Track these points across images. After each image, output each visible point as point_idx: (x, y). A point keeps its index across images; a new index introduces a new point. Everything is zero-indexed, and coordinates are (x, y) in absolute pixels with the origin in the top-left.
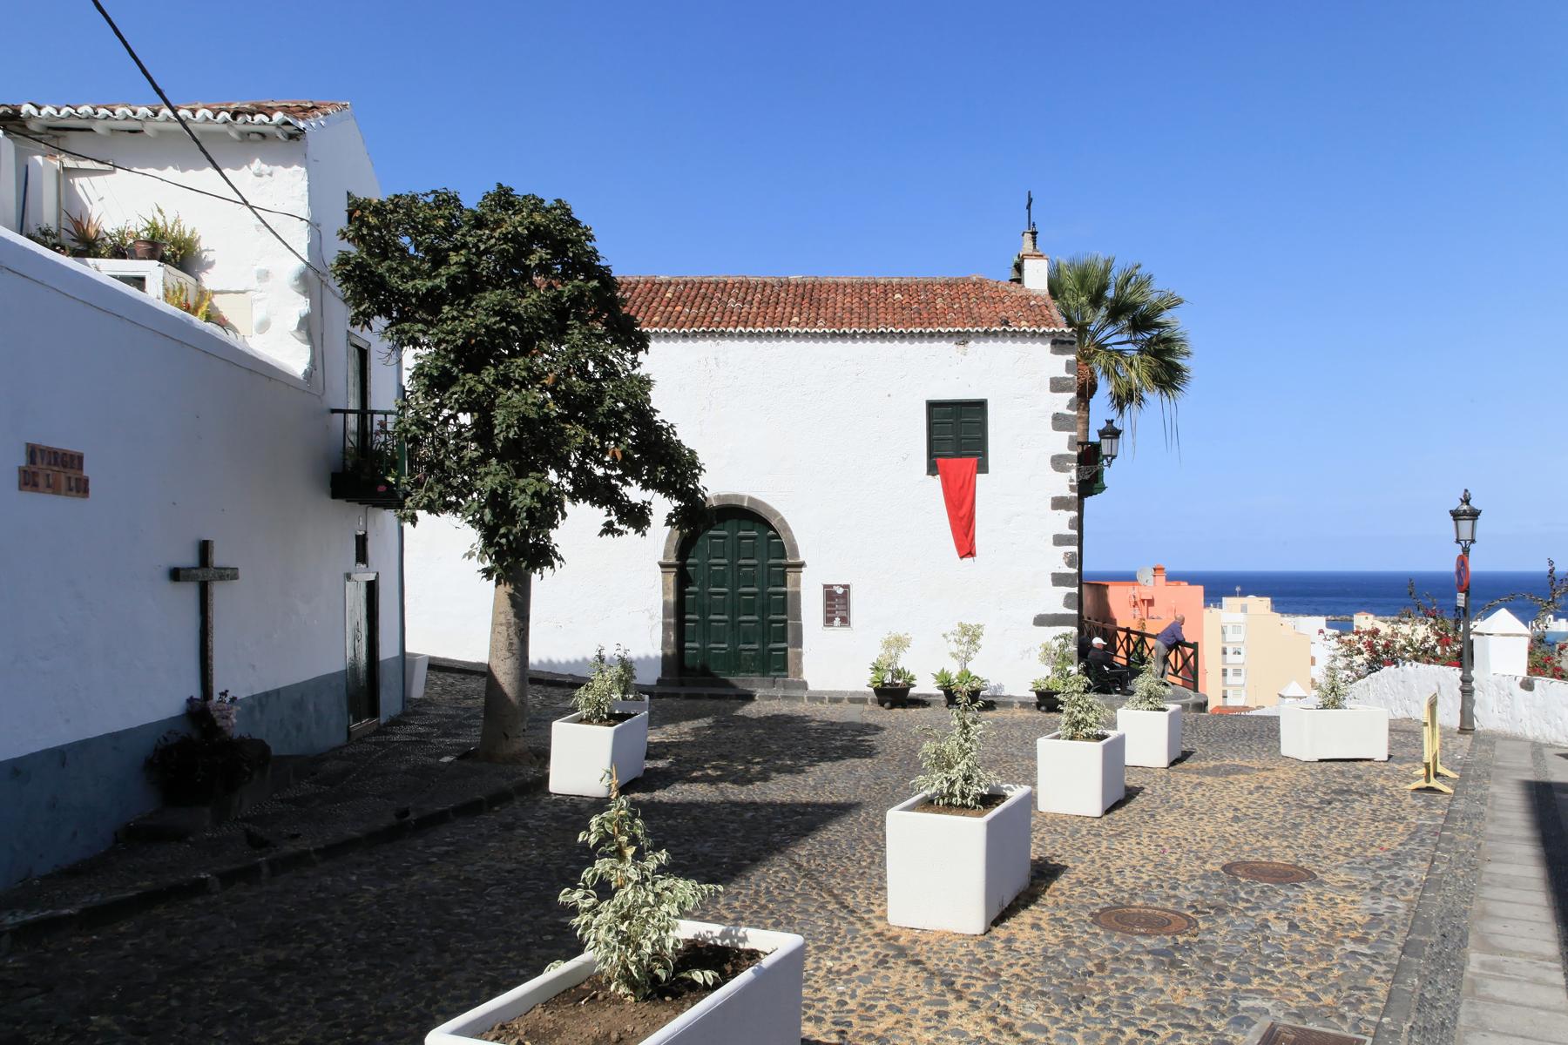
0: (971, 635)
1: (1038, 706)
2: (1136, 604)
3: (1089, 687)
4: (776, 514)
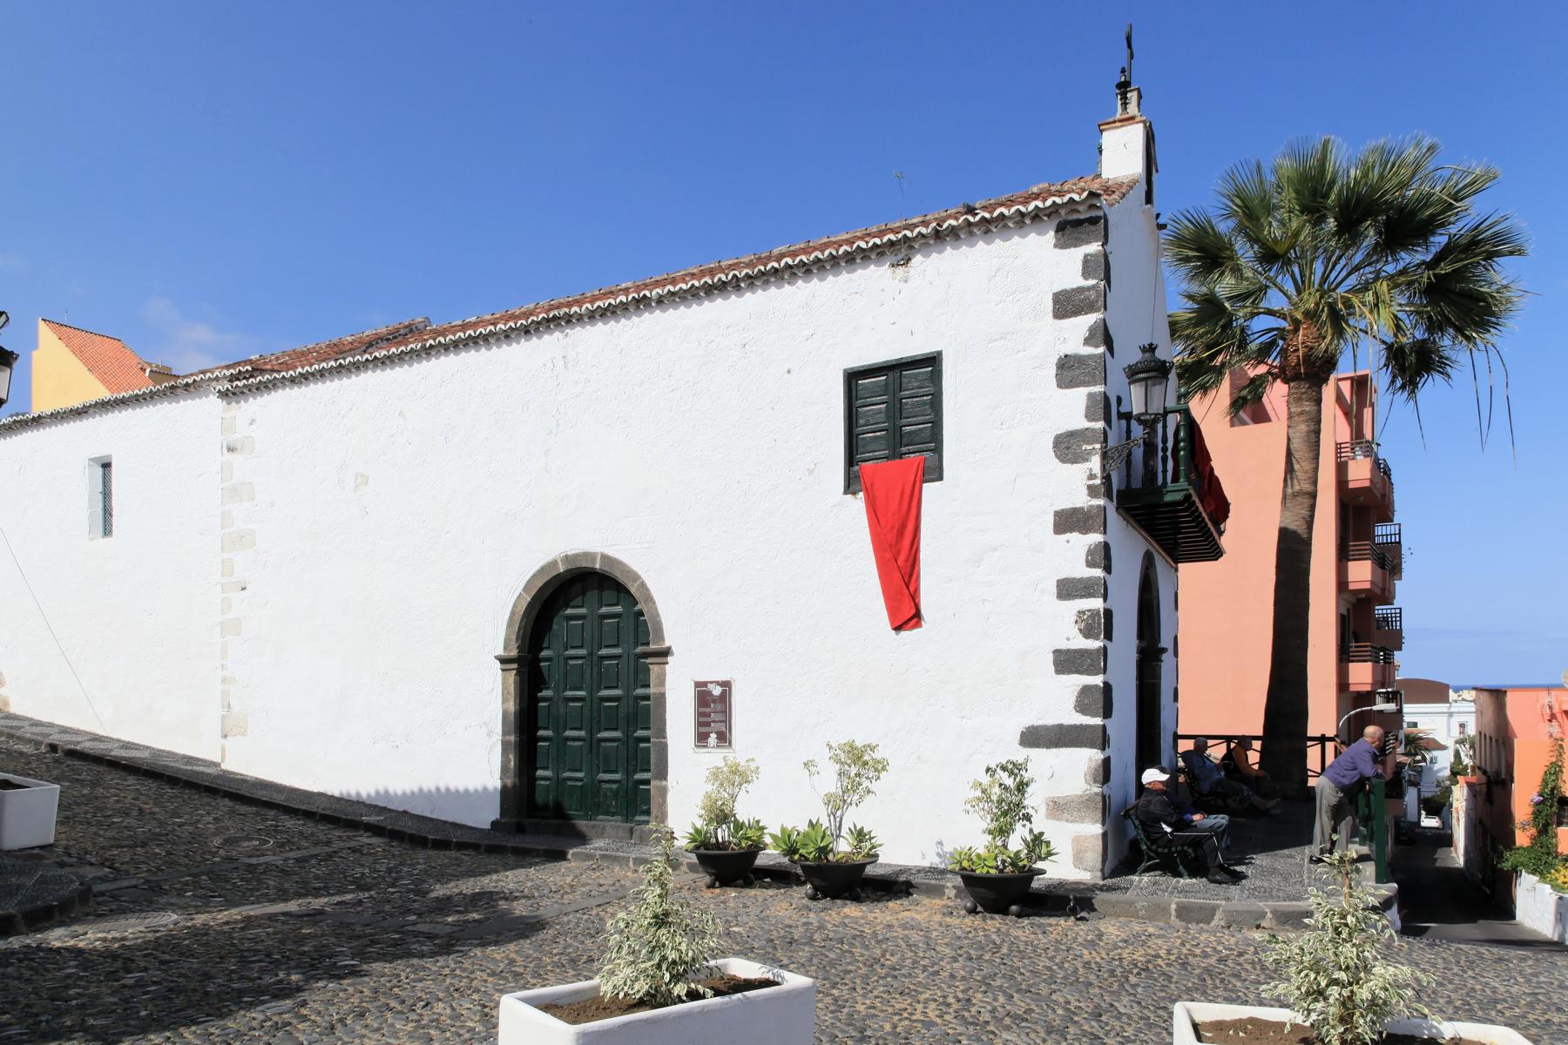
0: (859, 764)
2: (1553, 717)
4: (636, 577)
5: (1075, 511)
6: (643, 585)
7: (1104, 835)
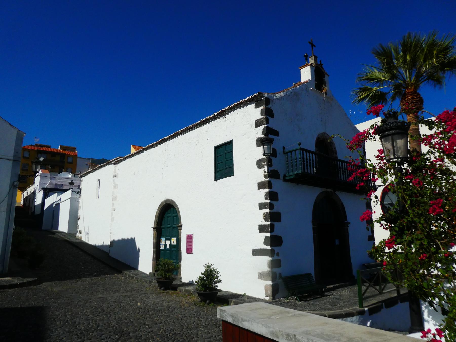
5: (262, 182)
7: (20, 207)
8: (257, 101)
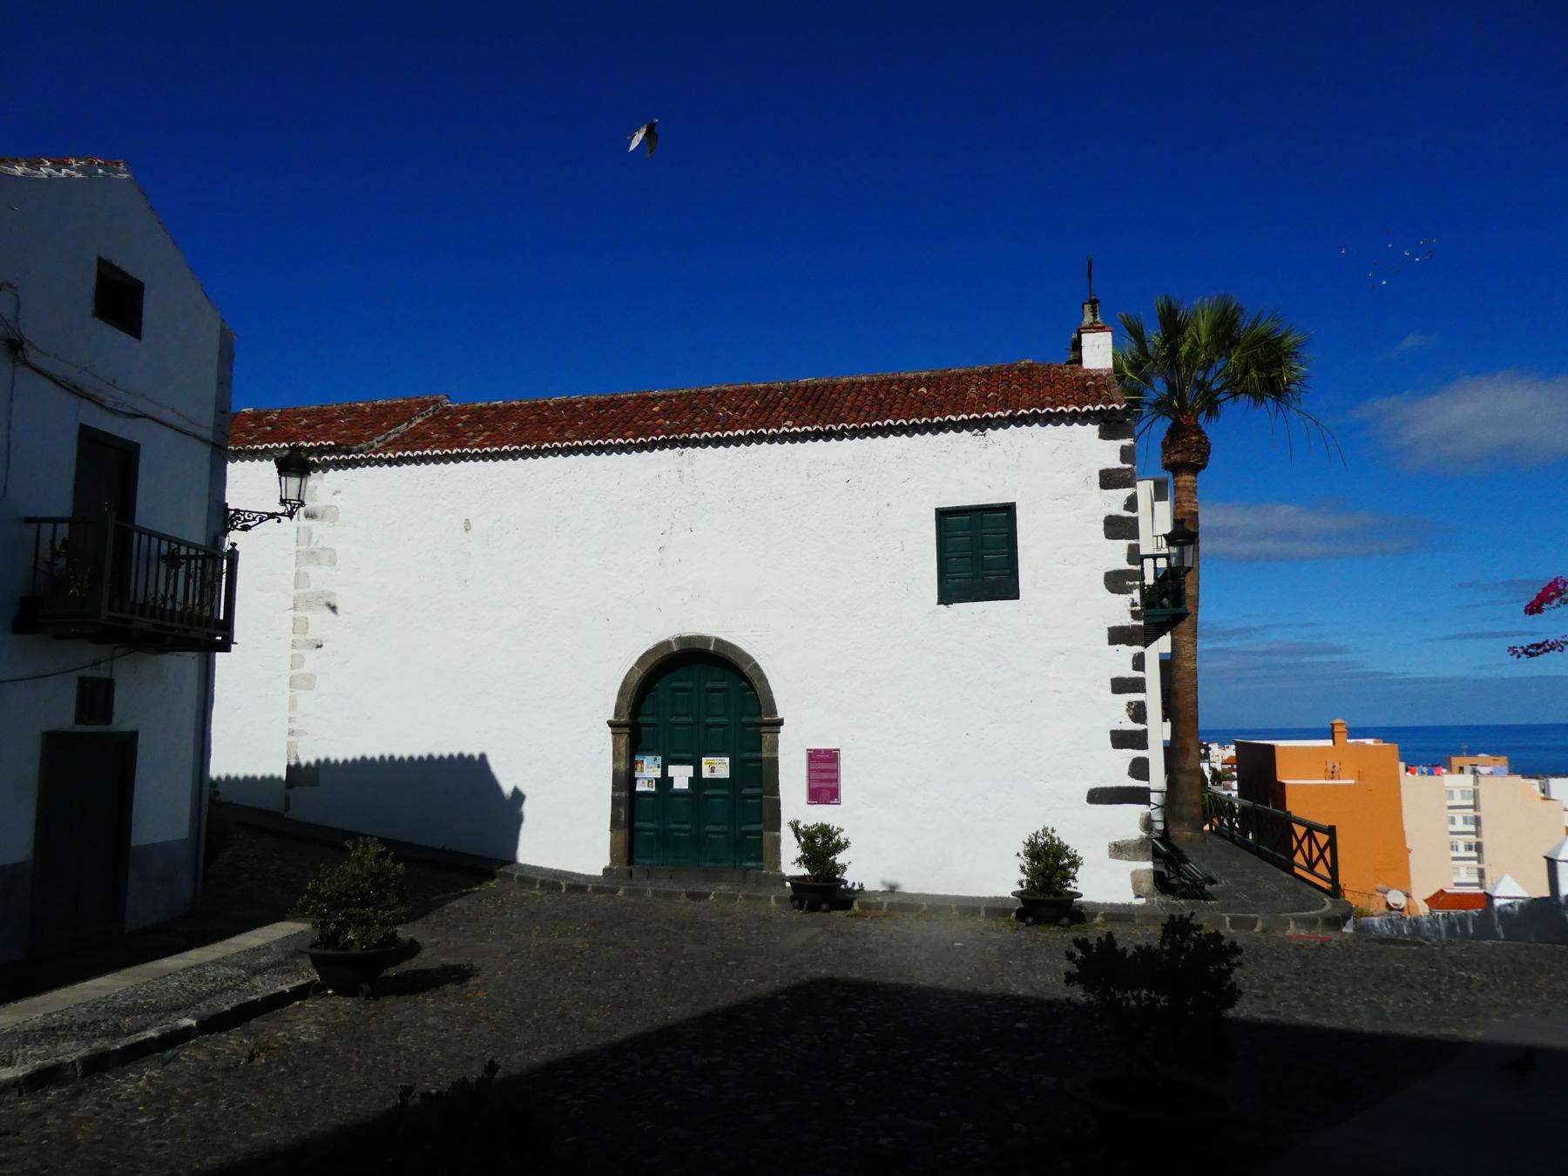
1: (1021, 915)
3: (287, 807)
4: (749, 659)
6: (756, 666)
8: (1107, 422)
